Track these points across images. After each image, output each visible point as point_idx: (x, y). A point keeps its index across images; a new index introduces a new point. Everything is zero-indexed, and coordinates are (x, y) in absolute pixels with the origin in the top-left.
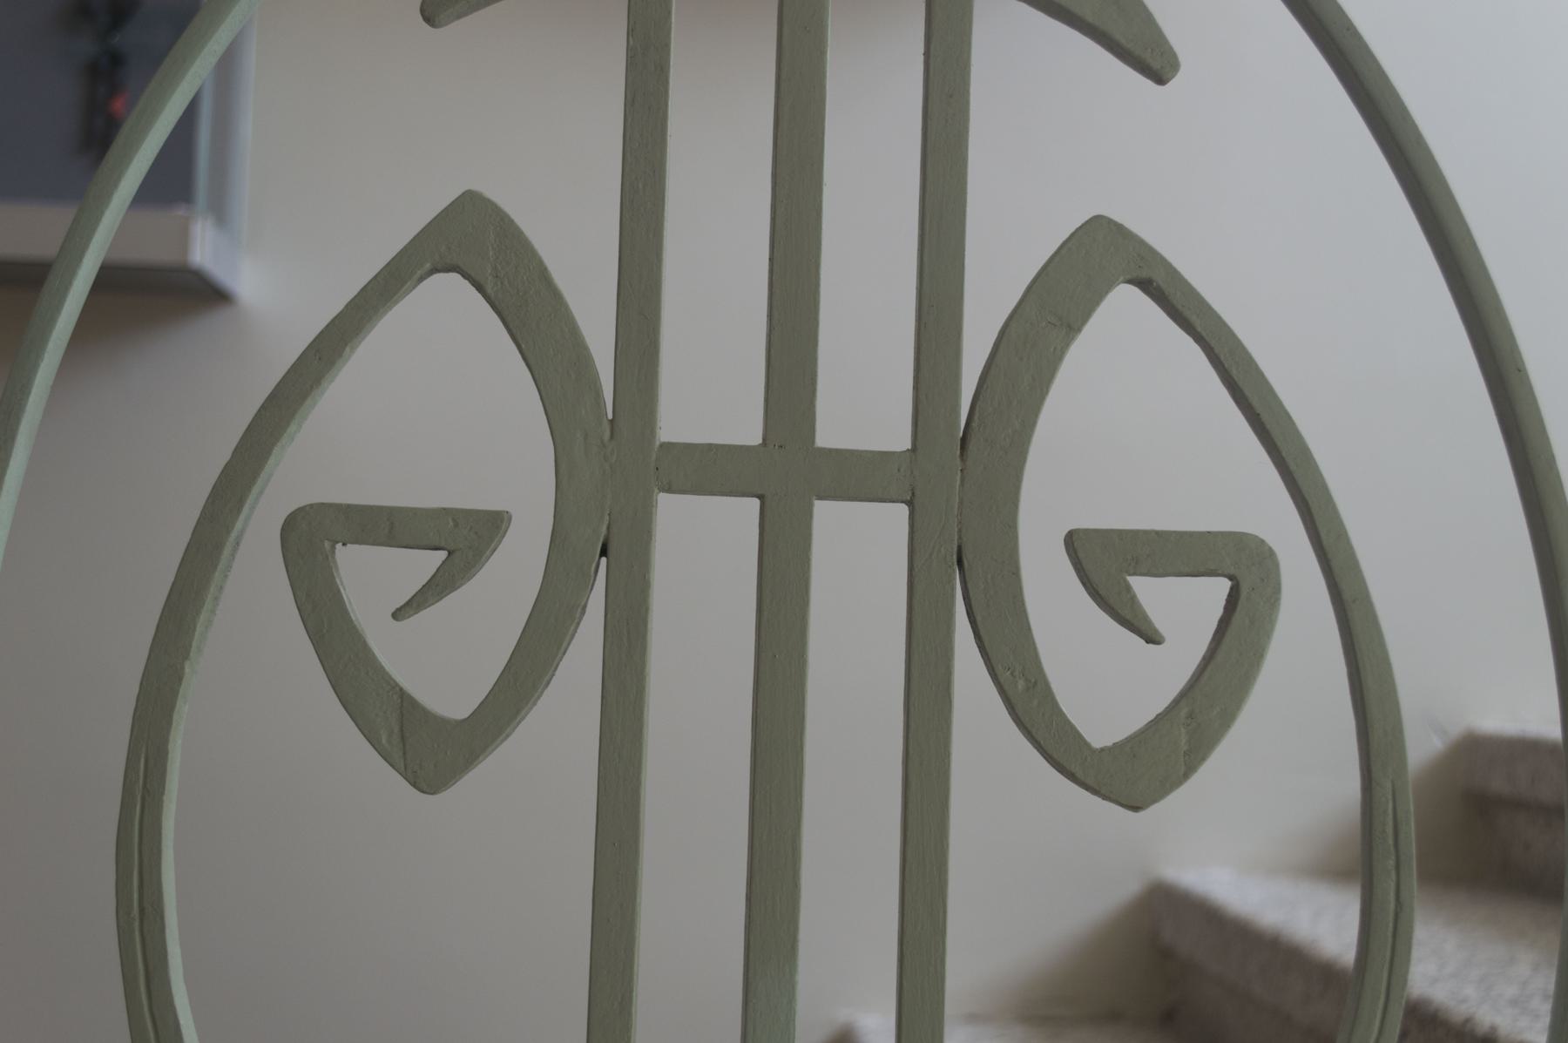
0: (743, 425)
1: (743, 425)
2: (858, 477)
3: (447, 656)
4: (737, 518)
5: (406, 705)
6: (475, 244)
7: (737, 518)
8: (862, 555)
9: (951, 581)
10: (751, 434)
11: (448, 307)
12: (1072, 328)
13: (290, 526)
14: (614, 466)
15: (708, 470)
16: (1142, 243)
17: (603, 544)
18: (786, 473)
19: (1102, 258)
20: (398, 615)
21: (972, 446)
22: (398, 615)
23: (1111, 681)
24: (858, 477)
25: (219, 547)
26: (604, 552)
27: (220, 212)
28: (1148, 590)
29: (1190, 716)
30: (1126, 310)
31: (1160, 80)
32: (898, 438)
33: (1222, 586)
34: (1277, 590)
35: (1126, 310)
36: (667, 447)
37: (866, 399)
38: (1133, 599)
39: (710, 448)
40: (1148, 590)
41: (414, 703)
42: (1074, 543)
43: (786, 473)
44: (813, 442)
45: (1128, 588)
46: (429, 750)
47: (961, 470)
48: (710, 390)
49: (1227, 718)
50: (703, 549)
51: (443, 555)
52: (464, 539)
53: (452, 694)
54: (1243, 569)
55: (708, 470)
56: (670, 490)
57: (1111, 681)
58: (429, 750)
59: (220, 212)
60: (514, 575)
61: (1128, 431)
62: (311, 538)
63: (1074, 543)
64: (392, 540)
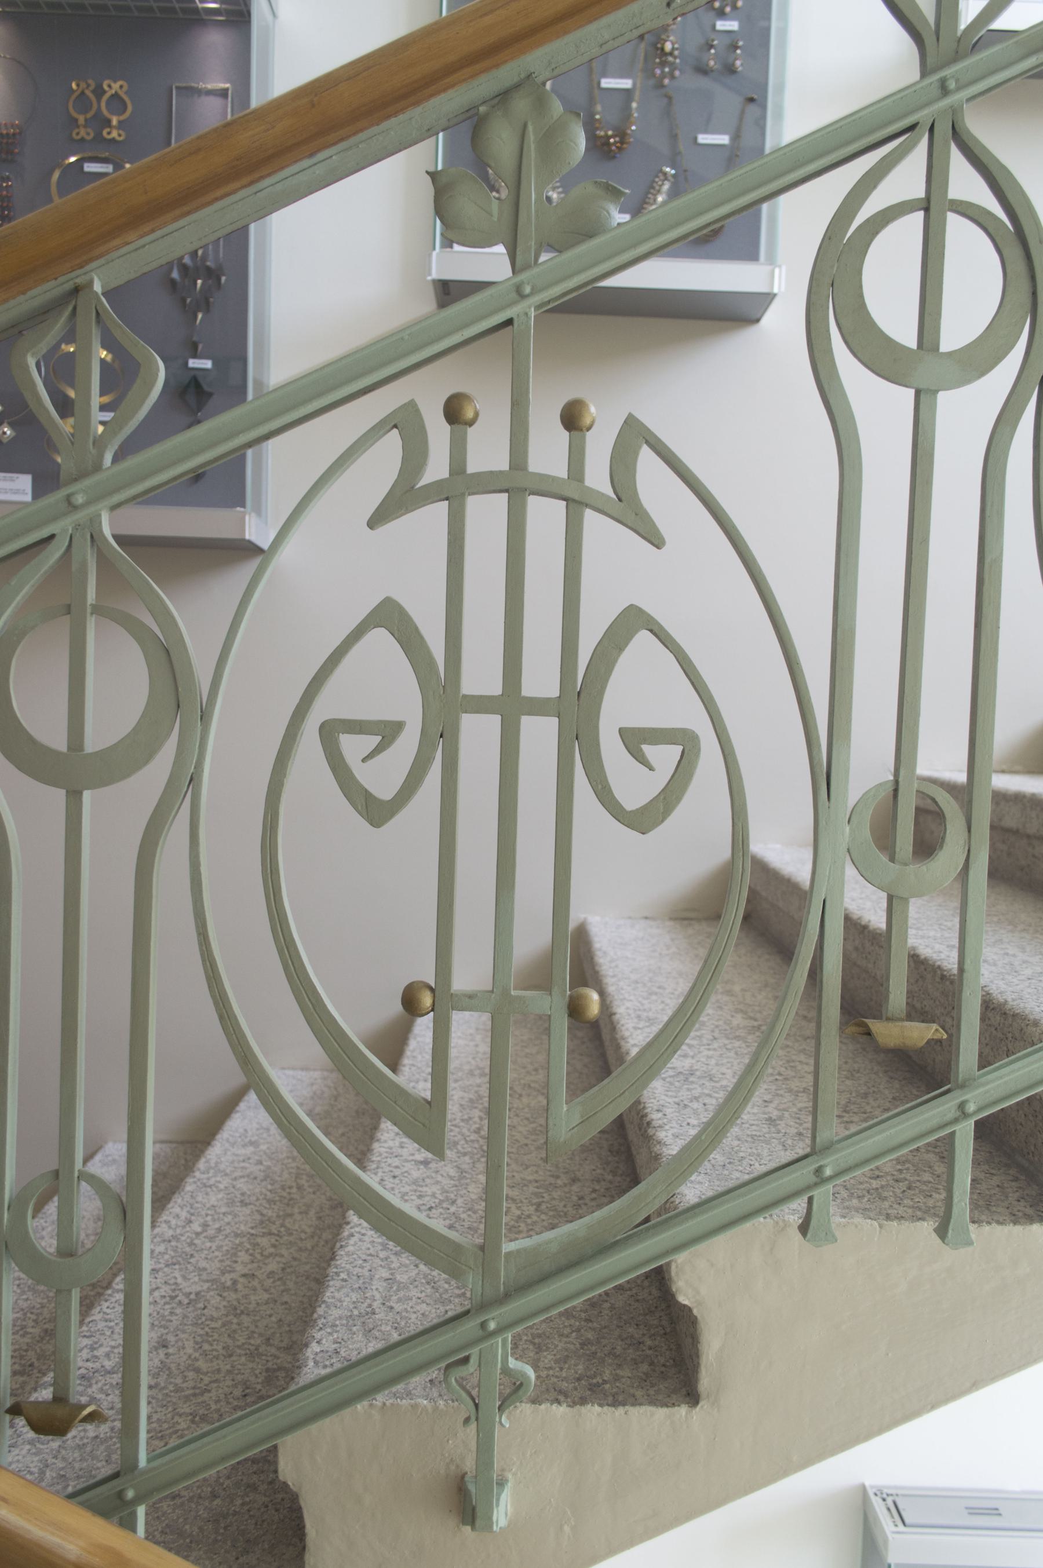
0: (495, 688)
1: (495, 688)
2: (538, 707)
3: (383, 777)
4: (493, 722)
5: (368, 795)
6: (390, 616)
7: (493, 722)
8: (540, 735)
9: (574, 746)
10: (498, 691)
11: (380, 638)
12: (621, 649)
13: (323, 727)
14: (445, 704)
15: (481, 705)
16: (649, 615)
17: (441, 735)
18: (511, 705)
19: (632, 621)
20: (364, 760)
21: (582, 695)
22: (364, 760)
23: (635, 786)
24: (538, 707)
25: (296, 735)
26: (441, 736)
27: (258, 510)
28: (647, 749)
29: (665, 798)
30: (643, 638)
31: (658, 548)
32: (555, 693)
33: (679, 749)
34: (699, 750)
35: (643, 638)
36: (465, 696)
37: (541, 679)
38: (643, 754)
39: (481, 696)
40: (647, 749)
41: (371, 794)
42: (622, 732)
43: (511, 705)
44: (449, 986)
45: (641, 750)
46: (376, 811)
47: (578, 707)
48: (481, 675)
49: (679, 799)
50: (480, 734)
51: (380, 738)
52: (388, 732)
53: (385, 790)
54: (687, 742)
55: (481, 705)
56: (466, 712)
57: (635, 786)
58: (376, 811)
59: (258, 510)
60: (408, 744)
61: (641, 691)
62: (330, 732)
63: (622, 732)
64: (361, 732)
